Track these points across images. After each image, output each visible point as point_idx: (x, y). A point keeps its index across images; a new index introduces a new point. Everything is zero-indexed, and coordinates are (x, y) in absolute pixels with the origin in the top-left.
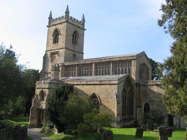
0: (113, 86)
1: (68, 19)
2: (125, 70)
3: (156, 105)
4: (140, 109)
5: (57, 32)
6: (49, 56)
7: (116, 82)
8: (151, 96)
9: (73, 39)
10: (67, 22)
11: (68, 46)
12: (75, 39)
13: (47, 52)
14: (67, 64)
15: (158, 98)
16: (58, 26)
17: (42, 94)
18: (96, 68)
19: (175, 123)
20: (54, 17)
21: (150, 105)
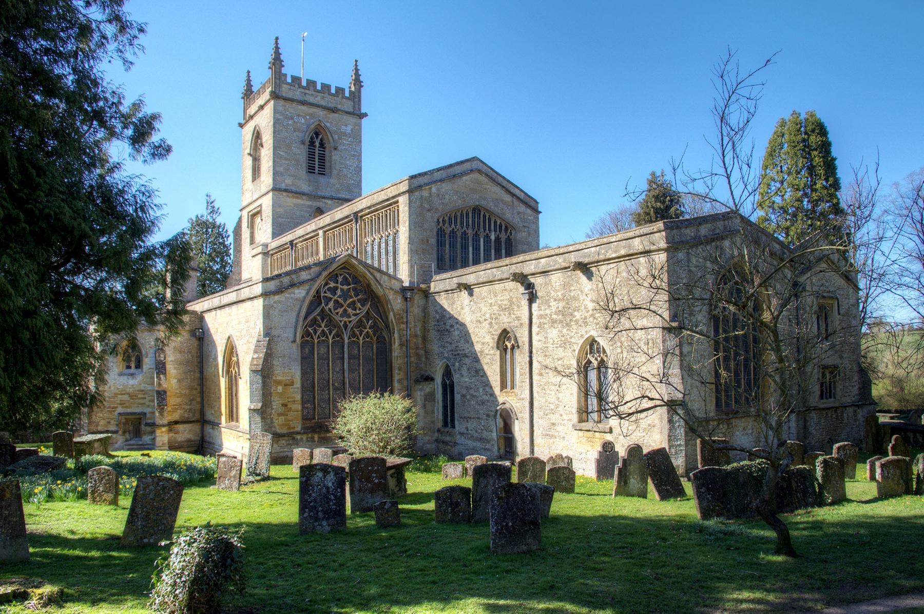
3: (468, 370)
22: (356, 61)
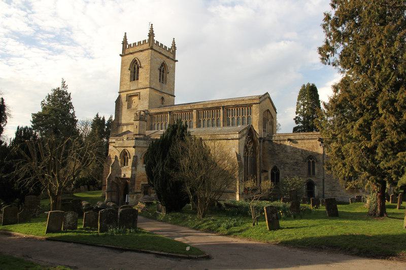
0: (231, 141)
1: (151, 43)
2: (248, 119)
4: (265, 174)
5: (137, 63)
6: (124, 99)
7: (237, 136)
8: (282, 156)
10: (152, 48)
11: (154, 84)
12: (163, 75)
13: (121, 94)
14: (152, 111)
15: (292, 159)
16: (136, 55)
17: (124, 155)
18: (198, 117)
19: (316, 194)
20: (130, 41)
21: (280, 169)
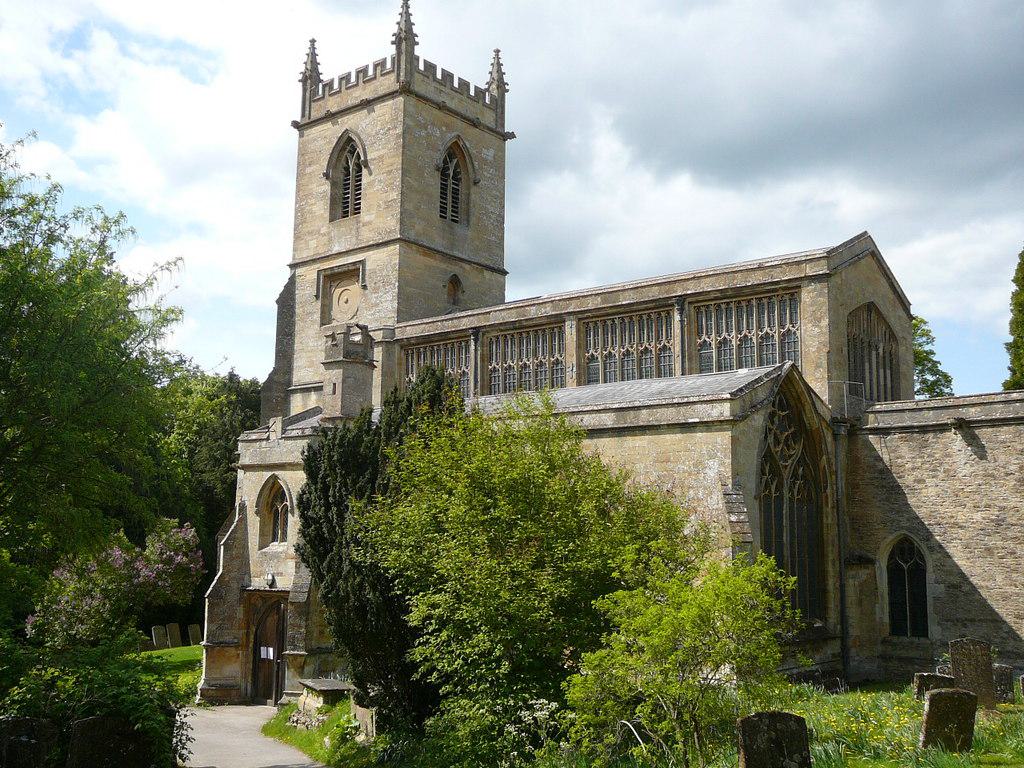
9: (444, 188)
22: (497, 51)
